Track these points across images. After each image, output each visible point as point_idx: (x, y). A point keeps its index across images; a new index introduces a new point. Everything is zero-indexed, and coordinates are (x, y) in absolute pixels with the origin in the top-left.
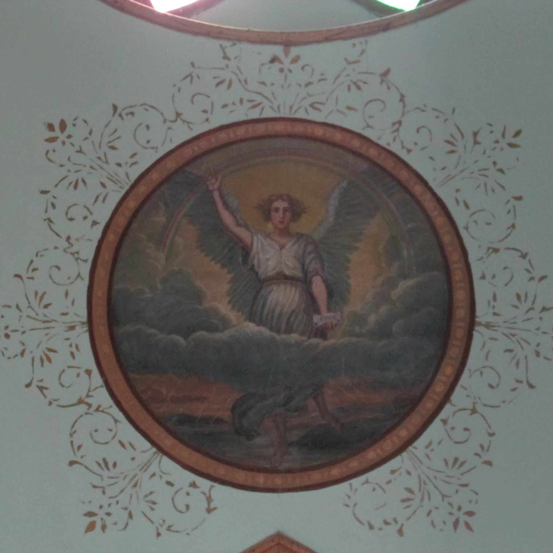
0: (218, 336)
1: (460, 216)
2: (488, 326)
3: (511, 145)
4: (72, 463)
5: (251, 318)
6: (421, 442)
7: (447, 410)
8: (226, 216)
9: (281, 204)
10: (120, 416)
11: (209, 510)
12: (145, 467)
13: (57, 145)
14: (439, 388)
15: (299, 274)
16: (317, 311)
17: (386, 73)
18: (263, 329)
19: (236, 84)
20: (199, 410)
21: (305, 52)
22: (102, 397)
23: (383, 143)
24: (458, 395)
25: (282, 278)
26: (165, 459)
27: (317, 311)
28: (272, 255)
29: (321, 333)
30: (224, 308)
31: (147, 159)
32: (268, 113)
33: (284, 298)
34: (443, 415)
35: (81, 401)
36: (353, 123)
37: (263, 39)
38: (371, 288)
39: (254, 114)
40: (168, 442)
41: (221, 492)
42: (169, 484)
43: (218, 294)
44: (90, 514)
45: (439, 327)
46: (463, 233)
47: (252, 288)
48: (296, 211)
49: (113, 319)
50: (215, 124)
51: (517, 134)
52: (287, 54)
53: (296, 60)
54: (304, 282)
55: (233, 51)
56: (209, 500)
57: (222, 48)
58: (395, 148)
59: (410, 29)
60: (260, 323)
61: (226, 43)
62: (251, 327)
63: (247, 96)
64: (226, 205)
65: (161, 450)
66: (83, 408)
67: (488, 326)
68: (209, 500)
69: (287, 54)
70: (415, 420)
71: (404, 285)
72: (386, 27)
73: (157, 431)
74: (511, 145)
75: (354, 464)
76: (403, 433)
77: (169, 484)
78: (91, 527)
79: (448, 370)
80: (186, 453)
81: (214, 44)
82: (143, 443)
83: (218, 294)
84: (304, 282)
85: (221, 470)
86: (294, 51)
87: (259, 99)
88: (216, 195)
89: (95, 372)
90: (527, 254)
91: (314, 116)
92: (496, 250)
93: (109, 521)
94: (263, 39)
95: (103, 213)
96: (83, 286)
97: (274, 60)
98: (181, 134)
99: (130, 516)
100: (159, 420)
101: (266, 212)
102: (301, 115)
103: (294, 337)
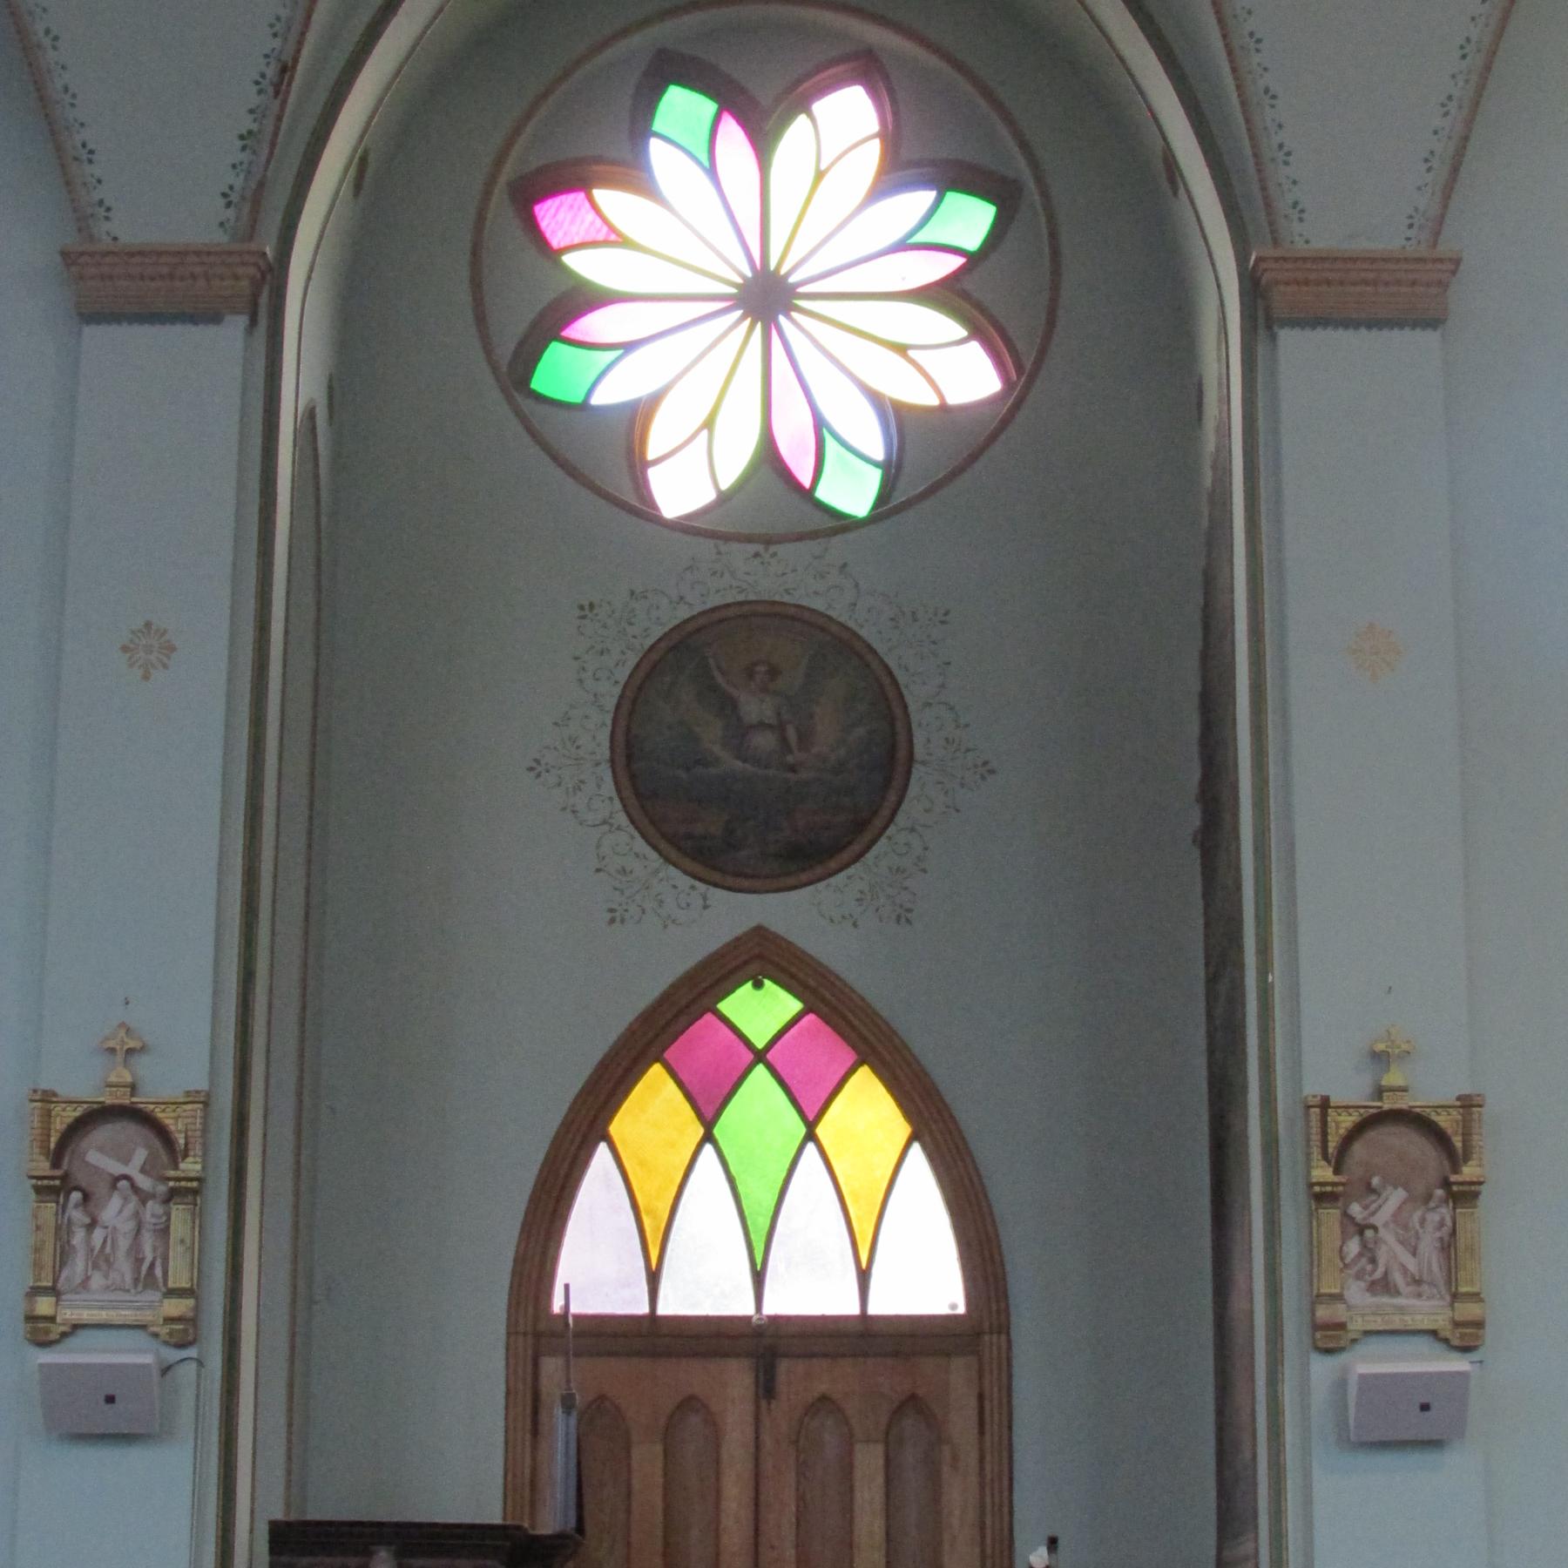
0: (713, 771)
1: (901, 678)
2: (923, 763)
3: (943, 622)
4: (598, 870)
5: (738, 758)
6: (870, 856)
7: (891, 830)
8: (720, 679)
9: (762, 669)
10: (636, 834)
11: (706, 907)
12: (657, 871)
13: (586, 622)
14: (885, 812)
15: (773, 721)
16: (790, 751)
17: (845, 565)
18: (748, 766)
19: (727, 575)
20: (699, 829)
21: (781, 549)
22: (622, 819)
23: (842, 619)
24: (900, 819)
25: (762, 726)
26: (671, 868)
27: (790, 751)
28: (754, 708)
29: (792, 769)
30: (716, 749)
31: (657, 632)
32: (752, 597)
33: (764, 742)
34: (889, 832)
35: (604, 822)
36: (818, 604)
37: (749, 539)
38: (832, 733)
39: (741, 598)
40: (673, 854)
41: (717, 895)
42: (675, 887)
43: (711, 734)
44: (612, 910)
45: (885, 765)
46: (905, 692)
47: (738, 733)
48: (774, 672)
49: (629, 757)
50: (709, 606)
51: (946, 614)
52: (766, 550)
53: (774, 554)
54: (780, 728)
55: (723, 548)
56: (705, 898)
57: (716, 546)
58: (851, 624)
59: (864, 531)
60: (745, 761)
61: (720, 542)
62: (739, 764)
63: (735, 584)
64: (719, 668)
65: (668, 860)
66: (606, 827)
67: (923, 763)
68: (705, 898)
69: (766, 550)
70: (866, 837)
71: (861, 731)
72: (835, 532)
73: (663, 845)
74: (943, 622)
75: (819, 870)
76: (856, 848)
77: (675, 887)
78: (612, 921)
79: (892, 797)
80: (687, 863)
81: (711, 543)
82: (654, 855)
83: (711, 734)
84: (780, 728)
85: (717, 877)
86: (773, 549)
87: (745, 586)
88: (711, 661)
89: (697, 884)
90: (165, 631)
91: (787, 599)
92: (930, 704)
93: (627, 916)
94: (749, 539)
95: (623, 674)
96: (607, 731)
97: (757, 555)
98: (684, 613)
99: (644, 912)
100: (664, 836)
101: (750, 673)
102: (777, 598)
103: (771, 772)
